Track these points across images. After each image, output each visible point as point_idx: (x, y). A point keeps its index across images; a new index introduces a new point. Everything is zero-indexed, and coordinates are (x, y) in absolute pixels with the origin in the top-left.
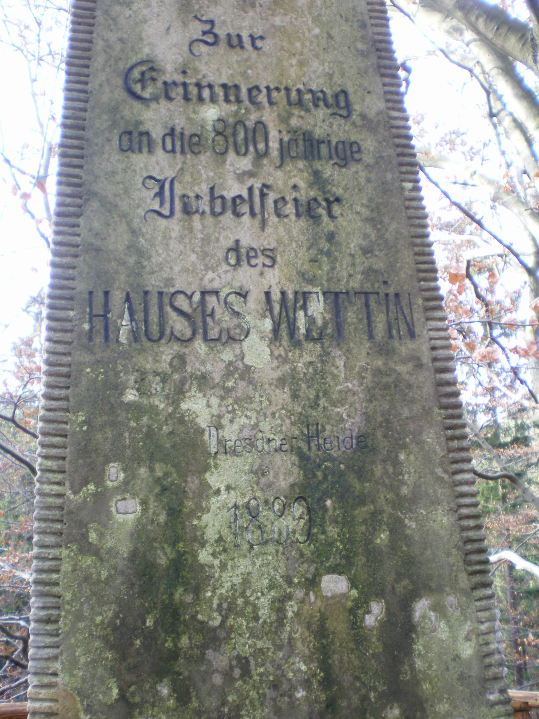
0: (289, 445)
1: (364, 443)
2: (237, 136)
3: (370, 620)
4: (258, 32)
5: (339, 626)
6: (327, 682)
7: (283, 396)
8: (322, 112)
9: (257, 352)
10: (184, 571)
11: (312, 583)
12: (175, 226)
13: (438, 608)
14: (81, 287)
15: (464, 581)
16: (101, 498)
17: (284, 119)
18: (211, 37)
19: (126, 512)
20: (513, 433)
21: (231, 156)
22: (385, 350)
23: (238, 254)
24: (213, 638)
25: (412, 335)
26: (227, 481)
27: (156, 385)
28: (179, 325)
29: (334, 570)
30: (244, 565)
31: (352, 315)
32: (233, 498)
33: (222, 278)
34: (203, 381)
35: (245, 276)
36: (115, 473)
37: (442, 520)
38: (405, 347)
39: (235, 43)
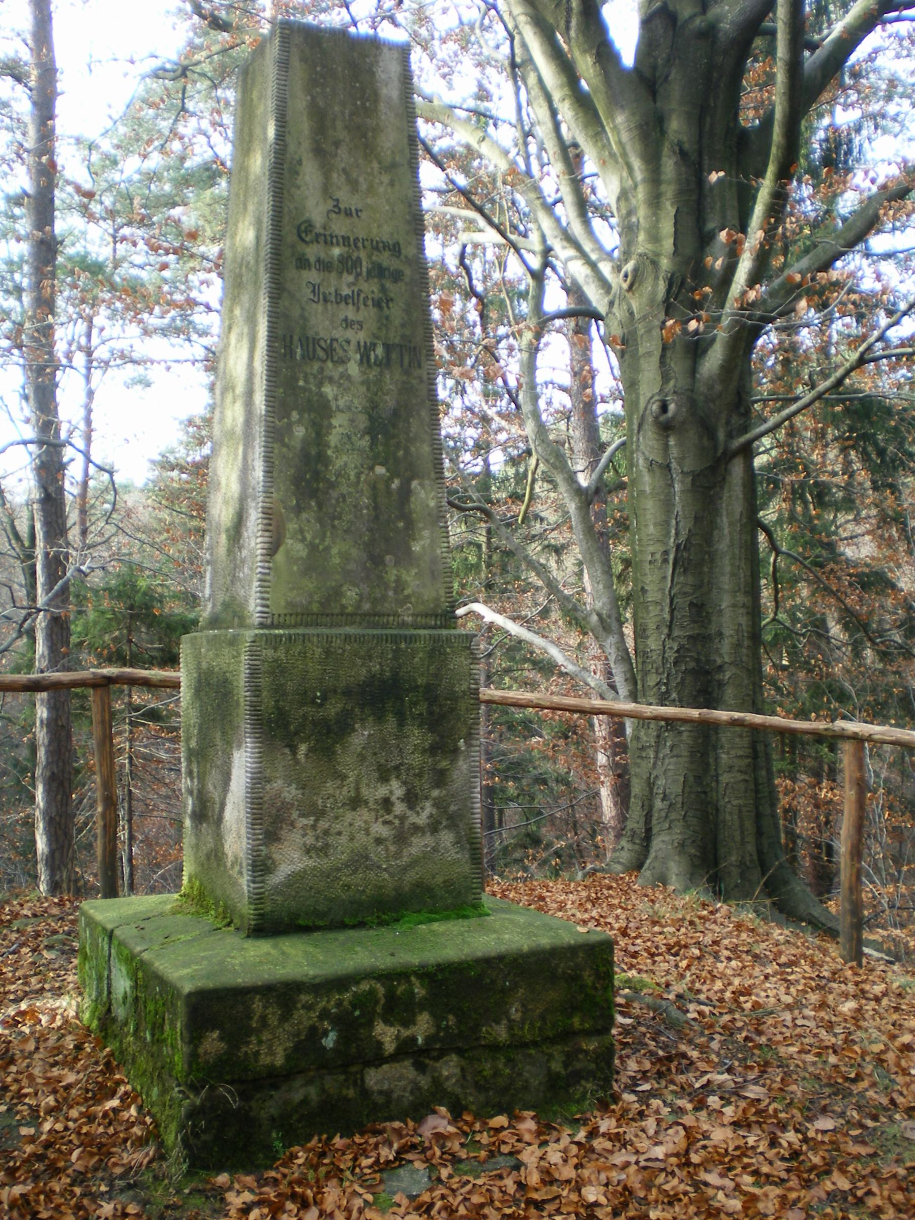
0: (366, 411)
1: (396, 413)
2: (348, 264)
3: (394, 486)
4: (359, 207)
5: (381, 486)
6: (376, 508)
7: (363, 389)
8: (387, 254)
9: (353, 369)
10: (322, 458)
11: (371, 468)
12: (319, 307)
13: (422, 485)
14: (280, 333)
15: (433, 475)
16: (290, 425)
17: (369, 256)
18: (337, 209)
19: (300, 432)
20: (512, 485)
21: (345, 275)
22: (407, 373)
23: (348, 323)
24: (332, 485)
25: (420, 367)
26: (339, 424)
27: (311, 380)
28: (321, 354)
29: (381, 464)
30: (345, 458)
31: (394, 356)
32: (341, 430)
33: (339, 333)
34: (331, 380)
35: (349, 334)
36: (295, 415)
37: (426, 449)
38: (416, 372)
39: (348, 213)
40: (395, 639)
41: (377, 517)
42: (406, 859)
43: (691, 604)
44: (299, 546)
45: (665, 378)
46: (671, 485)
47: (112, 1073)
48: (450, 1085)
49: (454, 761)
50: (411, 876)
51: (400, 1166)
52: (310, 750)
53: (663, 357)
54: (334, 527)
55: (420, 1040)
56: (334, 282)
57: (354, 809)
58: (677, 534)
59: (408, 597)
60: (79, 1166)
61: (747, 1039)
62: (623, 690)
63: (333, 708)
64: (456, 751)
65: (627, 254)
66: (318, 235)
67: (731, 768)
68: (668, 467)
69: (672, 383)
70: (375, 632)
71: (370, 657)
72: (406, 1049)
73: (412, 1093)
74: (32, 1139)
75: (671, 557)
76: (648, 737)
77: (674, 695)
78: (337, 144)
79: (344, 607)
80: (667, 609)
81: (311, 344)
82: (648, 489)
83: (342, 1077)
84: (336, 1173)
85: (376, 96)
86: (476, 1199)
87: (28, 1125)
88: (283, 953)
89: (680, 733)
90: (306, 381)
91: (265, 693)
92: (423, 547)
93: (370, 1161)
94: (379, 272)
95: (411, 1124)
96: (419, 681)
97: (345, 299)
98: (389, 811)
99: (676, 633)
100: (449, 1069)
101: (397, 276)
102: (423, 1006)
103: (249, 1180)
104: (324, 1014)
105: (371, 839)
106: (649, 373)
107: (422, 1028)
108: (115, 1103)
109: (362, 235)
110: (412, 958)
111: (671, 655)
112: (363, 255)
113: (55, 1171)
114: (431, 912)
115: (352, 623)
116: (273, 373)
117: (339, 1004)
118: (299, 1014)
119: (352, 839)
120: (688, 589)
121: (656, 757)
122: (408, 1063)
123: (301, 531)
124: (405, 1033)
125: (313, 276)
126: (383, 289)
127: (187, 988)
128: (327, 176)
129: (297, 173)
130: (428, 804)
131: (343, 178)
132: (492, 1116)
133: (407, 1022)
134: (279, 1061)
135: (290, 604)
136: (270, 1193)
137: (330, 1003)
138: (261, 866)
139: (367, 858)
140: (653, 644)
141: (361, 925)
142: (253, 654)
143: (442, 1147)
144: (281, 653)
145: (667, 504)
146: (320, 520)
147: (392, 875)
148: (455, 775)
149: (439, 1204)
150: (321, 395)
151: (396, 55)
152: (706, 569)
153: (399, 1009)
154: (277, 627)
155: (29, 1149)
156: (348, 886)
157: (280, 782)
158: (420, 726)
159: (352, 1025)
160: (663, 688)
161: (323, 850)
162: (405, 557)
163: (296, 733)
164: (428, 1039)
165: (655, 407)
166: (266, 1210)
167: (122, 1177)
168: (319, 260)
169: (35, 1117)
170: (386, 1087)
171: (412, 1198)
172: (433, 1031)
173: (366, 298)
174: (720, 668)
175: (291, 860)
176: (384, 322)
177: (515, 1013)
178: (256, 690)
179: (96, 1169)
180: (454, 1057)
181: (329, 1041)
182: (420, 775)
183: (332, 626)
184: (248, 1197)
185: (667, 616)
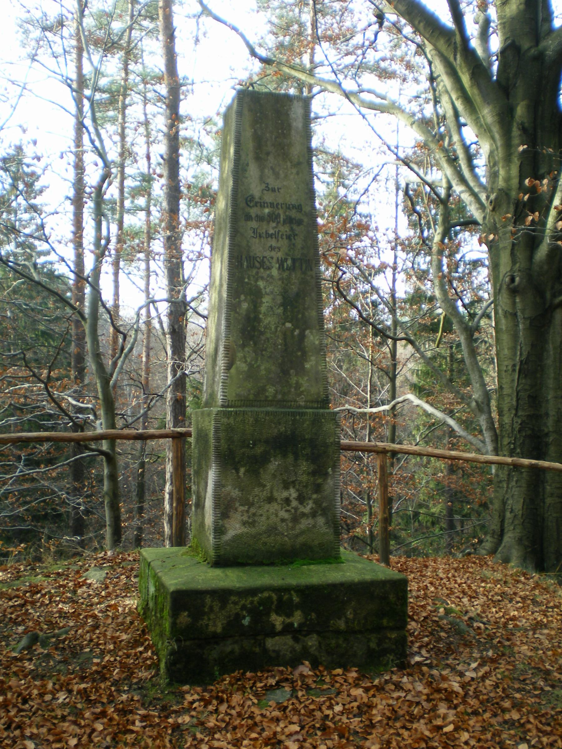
1: (298, 295)
2: (273, 217)
6: (286, 345)
7: (280, 283)
8: (294, 211)
9: (275, 272)
10: (257, 319)
11: (284, 324)
12: (257, 240)
13: (311, 333)
15: (318, 327)
16: (240, 302)
17: (285, 213)
19: (245, 306)
22: (304, 273)
23: (272, 248)
24: (262, 333)
25: (311, 270)
26: (266, 301)
28: (257, 264)
31: (297, 264)
33: (267, 254)
34: (262, 278)
35: (273, 254)
36: (243, 297)
38: (309, 273)
39: (273, 190)
40: (293, 414)
41: (286, 350)
42: (297, 531)
43: (529, 396)
44: (244, 365)
45: (514, 262)
46: (517, 326)
47: (145, 635)
48: (313, 650)
49: (325, 480)
50: (301, 540)
51: (278, 689)
52: (246, 471)
53: (512, 249)
54: (262, 355)
55: (296, 625)
56: (265, 227)
57: (270, 503)
58: (521, 354)
59: (302, 392)
60: (116, 677)
61: (499, 642)
62: (490, 447)
63: (259, 450)
64: (326, 474)
65: (492, 191)
66: (257, 203)
67: (552, 495)
68: (515, 315)
69: (518, 265)
70: (283, 410)
71: (280, 424)
72: (288, 629)
73: (291, 652)
74: (98, 664)
75: (518, 368)
76: (503, 475)
77: (518, 450)
78: (268, 154)
79: (267, 397)
80: (515, 399)
81: (251, 259)
82: (504, 328)
83: (253, 641)
84: (242, 689)
85: (289, 126)
86: (312, 707)
87: (98, 658)
88: (226, 575)
89: (522, 473)
90: (249, 278)
91: (222, 441)
92: (312, 366)
93: (262, 684)
94: (290, 221)
95: (289, 669)
96: (307, 437)
97: (271, 236)
98: (289, 505)
99: (520, 413)
100: (312, 641)
101: (299, 222)
102: (297, 607)
103: (199, 689)
104: (244, 607)
105: (278, 519)
106: (505, 259)
107: (297, 619)
108: (141, 649)
109: (280, 201)
110: (293, 582)
111: (517, 427)
112: (281, 212)
113: (104, 679)
114: (311, 559)
115: (271, 406)
116: (231, 274)
117: (252, 602)
118: (230, 606)
119: (268, 518)
120: (527, 387)
121: (508, 487)
122: (289, 637)
123: (245, 357)
124: (288, 621)
125: (253, 224)
126: (292, 230)
127: (172, 589)
128: (262, 171)
129: (246, 171)
130: (310, 502)
131: (271, 172)
132: (335, 669)
133: (289, 615)
134: (219, 630)
135: (237, 395)
136: (207, 695)
137: (247, 601)
138: (219, 530)
139: (276, 529)
140: (507, 420)
141: (272, 564)
142: (216, 420)
143: (303, 682)
144: (231, 421)
145: (515, 337)
146: (255, 352)
147: (290, 539)
148: (326, 487)
149: (290, 707)
150: (257, 287)
151: (301, 104)
152: (538, 375)
153: (284, 608)
154: (231, 407)
155: (94, 668)
156: (265, 544)
157: (230, 487)
158: (307, 460)
159: (260, 613)
160: (512, 446)
161: (252, 524)
162: (301, 371)
163: (239, 462)
164: (300, 625)
165: (507, 279)
166: (202, 703)
167: (136, 683)
168: (257, 216)
169: (103, 653)
170: (277, 648)
171: (278, 703)
172: (303, 620)
173: (282, 235)
174: (547, 435)
175: (235, 528)
176: (292, 246)
177: (350, 614)
178: (218, 439)
179: (125, 679)
180: (315, 636)
181: (246, 621)
182: (306, 487)
183: (260, 407)
184: (196, 697)
185: (514, 403)
